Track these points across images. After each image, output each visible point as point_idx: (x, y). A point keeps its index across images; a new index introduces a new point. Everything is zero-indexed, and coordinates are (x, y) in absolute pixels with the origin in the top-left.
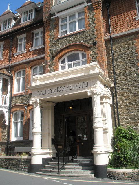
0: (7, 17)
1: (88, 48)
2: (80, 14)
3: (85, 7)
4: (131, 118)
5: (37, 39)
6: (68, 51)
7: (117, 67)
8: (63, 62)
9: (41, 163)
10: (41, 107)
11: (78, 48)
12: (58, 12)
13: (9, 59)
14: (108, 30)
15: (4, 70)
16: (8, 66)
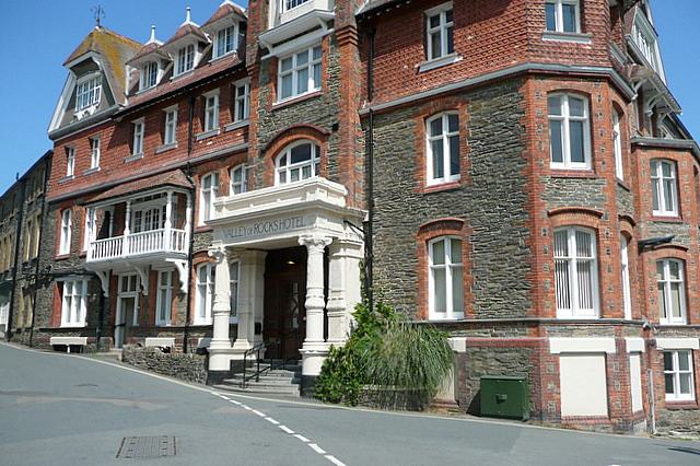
0: (185, 42)
1: (324, 137)
2: (318, 49)
3: (324, 37)
4: (394, 288)
6: (289, 138)
7: (379, 178)
8: (283, 162)
9: (228, 369)
10: (233, 267)
11: (303, 140)
12: (275, 46)
13: (190, 149)
14: (369, 94)
15: (178, 171)
16: (186, 163)
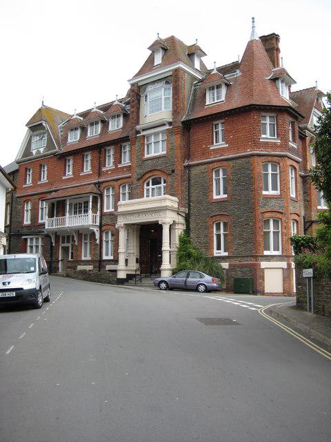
5: (125, 153)
9: (125, 277)
12: (143, 130)
